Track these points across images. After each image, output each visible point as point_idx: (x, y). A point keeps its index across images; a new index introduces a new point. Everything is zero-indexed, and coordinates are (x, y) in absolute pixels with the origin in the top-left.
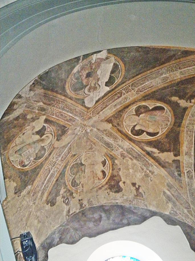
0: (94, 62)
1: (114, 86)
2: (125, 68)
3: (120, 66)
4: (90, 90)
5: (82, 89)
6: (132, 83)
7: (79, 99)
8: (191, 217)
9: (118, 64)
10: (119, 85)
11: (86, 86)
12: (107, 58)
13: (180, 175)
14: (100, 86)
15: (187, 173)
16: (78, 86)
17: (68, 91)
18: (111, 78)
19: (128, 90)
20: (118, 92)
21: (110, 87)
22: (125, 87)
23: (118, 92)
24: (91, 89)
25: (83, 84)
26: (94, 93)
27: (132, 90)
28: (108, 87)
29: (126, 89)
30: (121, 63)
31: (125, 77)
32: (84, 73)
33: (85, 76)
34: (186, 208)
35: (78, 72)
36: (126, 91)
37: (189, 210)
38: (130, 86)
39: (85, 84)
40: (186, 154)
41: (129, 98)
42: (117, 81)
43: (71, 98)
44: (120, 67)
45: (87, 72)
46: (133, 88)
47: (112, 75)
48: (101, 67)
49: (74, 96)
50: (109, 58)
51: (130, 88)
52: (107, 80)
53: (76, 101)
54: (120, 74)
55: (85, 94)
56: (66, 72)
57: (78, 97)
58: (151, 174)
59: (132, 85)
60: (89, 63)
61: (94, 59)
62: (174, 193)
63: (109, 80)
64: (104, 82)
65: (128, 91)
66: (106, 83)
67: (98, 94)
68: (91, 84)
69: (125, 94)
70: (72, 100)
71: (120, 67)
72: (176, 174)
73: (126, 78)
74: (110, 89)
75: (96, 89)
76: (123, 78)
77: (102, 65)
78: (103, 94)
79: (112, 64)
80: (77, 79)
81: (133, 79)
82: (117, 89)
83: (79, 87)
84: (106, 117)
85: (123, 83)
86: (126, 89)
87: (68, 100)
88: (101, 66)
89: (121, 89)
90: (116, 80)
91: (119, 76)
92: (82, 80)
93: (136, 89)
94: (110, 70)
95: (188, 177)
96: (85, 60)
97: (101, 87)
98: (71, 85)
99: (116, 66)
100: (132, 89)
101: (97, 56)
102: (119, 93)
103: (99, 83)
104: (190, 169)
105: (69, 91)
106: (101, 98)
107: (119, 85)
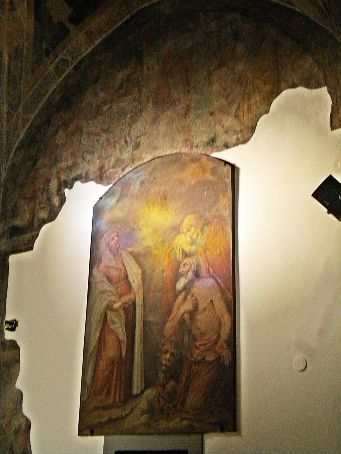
8: (5, 123)
13: (48, 53)
15: (61, 60)
34: (10, 105)
37: (13, 112)
40: (87, 33)
58: (8, 7)
72: (45, 46)
95: (57, 67)
104: (70, 59)
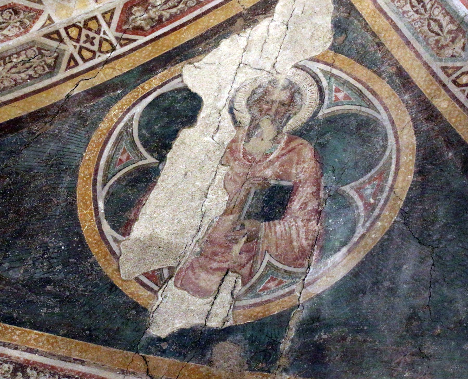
0: (231, 277)
1: (155, 81)
2: (72, 191)
3: (96, 208)
4: (284, 96)
5: (331, 121)
6: (55, 79)
7: (362, 58)
9: (106, 227)
10: (122, 84)
11: (302, 133)
12: (157, 279)
14: (231, 111)
16: (345, 152)
17: (409, 138)
18: (161, 144)
19: (83, 38)
20: (141, 40)
21: (175, 84)
22: (97, 61)
23: (141, 40)
24: (282, 104)
25: (319, 158)
26: (268, 67)
27: (63, 34)
28: (186, 89)
29: (95, 48)
30: (87, 226)
31: (87, 123)
32: (295, 226)
33: (295, 205)
35: (322, 244)
36: (98, 32)
38: (72, 57)
39: (308, 152)
41: (50, 18)
42: (129, 113)
43: (403, 81)
44: (101, 205)
45: (279, 227)
46: (54, 44)
47: (150, 160)
48: (204, 230)
49: (383, 88)
50: (144, 274)
51: (70, 48)
52: (187, 135)
53: (379, 55)
54: (109, 163)
55: (318, 82)
56: (393, 280)
57: (363, 72)
59: (53, 68)
60: (260, 280)
61: (225, 296)
62: (417, 221)
63: (175, 135)
64: (206, 126)
65: (84, 32)
66: (191, 120)
67: (252, 57)
68: (275, 140)
69: (104, 15)
70: (401, 72)
71: (101, 205)
73: (83, 118)
74: (178, 66)
75: (253, 92)
76: (95, 125)
77: (189, 245)
78: (225, 44)
79: (139, 230)
80: (342, 202)
81: (47, 103)
82: (142, 58)
83: (339, 137)
84: (256, 80)
85: (97, 92)
86: (95, 48)
87: (419, 77)
88: (200, 235)
89: (120, 50)
90: (136, 118)
91: (115, 144)
92: (318, 185)
93: (36, 30)
94: (155, 196)
96: (275, 310)
97: (222, 102)
98: (382, 175)
99: (126, 201)
100: (61, 40)
101: (208, 307)
102: (139, 30)
103: (228, 132)
105: (402, 142)
106: (240, 22)
107: (122, 84)
